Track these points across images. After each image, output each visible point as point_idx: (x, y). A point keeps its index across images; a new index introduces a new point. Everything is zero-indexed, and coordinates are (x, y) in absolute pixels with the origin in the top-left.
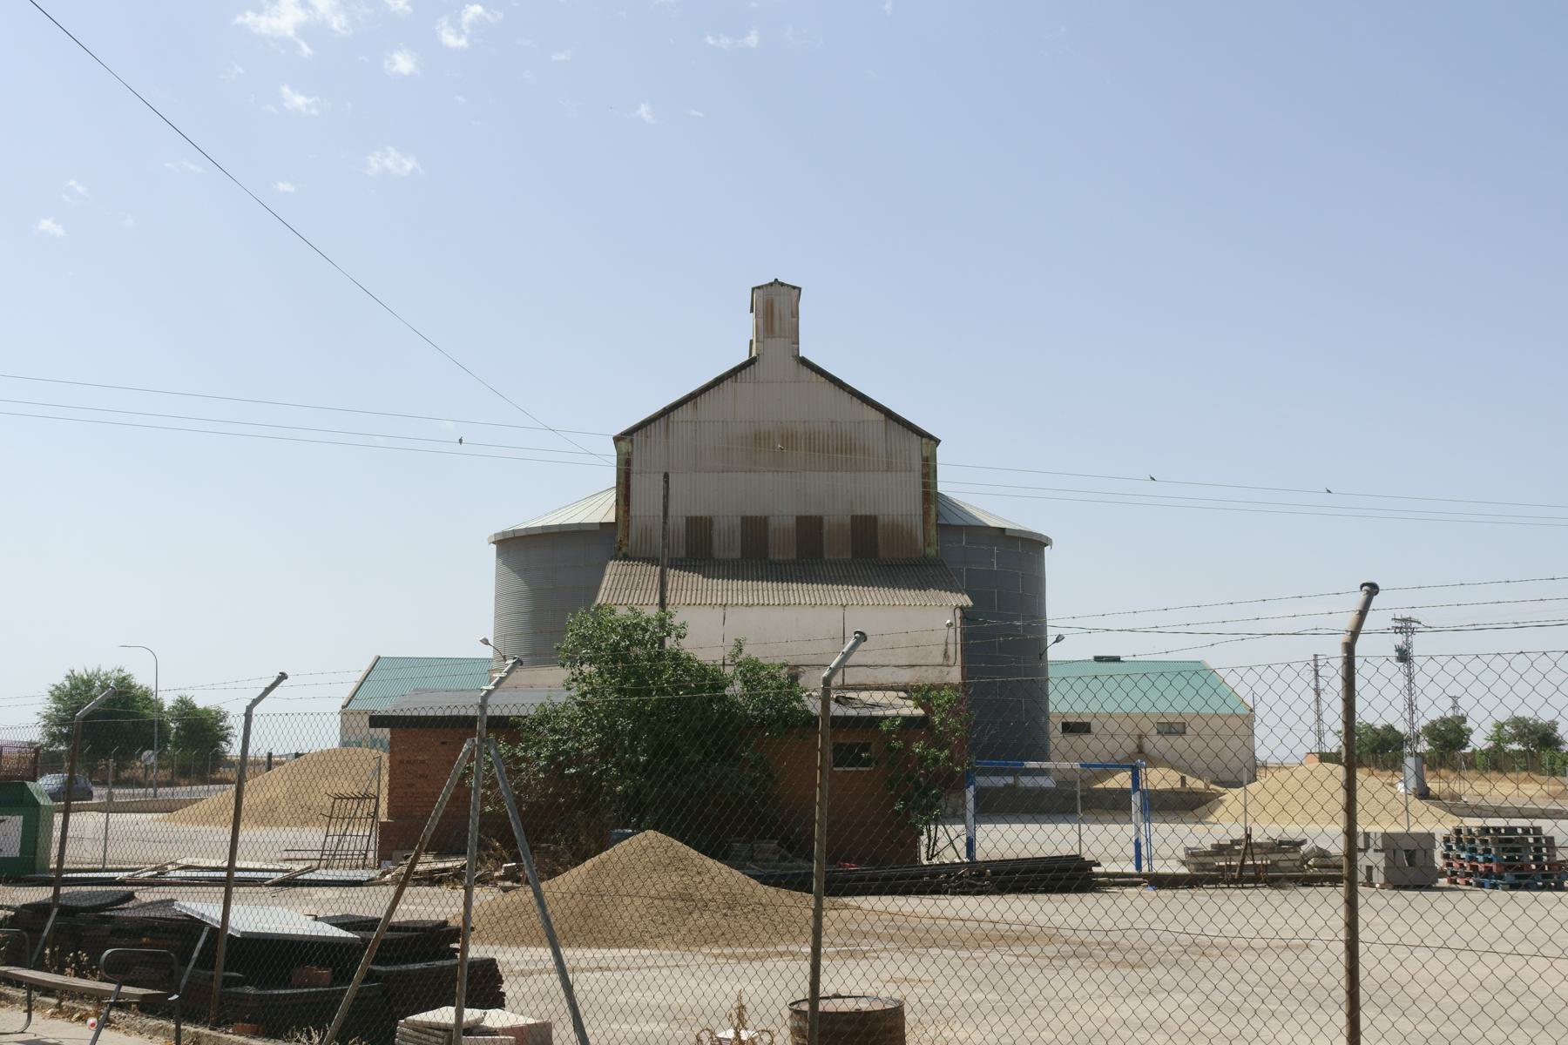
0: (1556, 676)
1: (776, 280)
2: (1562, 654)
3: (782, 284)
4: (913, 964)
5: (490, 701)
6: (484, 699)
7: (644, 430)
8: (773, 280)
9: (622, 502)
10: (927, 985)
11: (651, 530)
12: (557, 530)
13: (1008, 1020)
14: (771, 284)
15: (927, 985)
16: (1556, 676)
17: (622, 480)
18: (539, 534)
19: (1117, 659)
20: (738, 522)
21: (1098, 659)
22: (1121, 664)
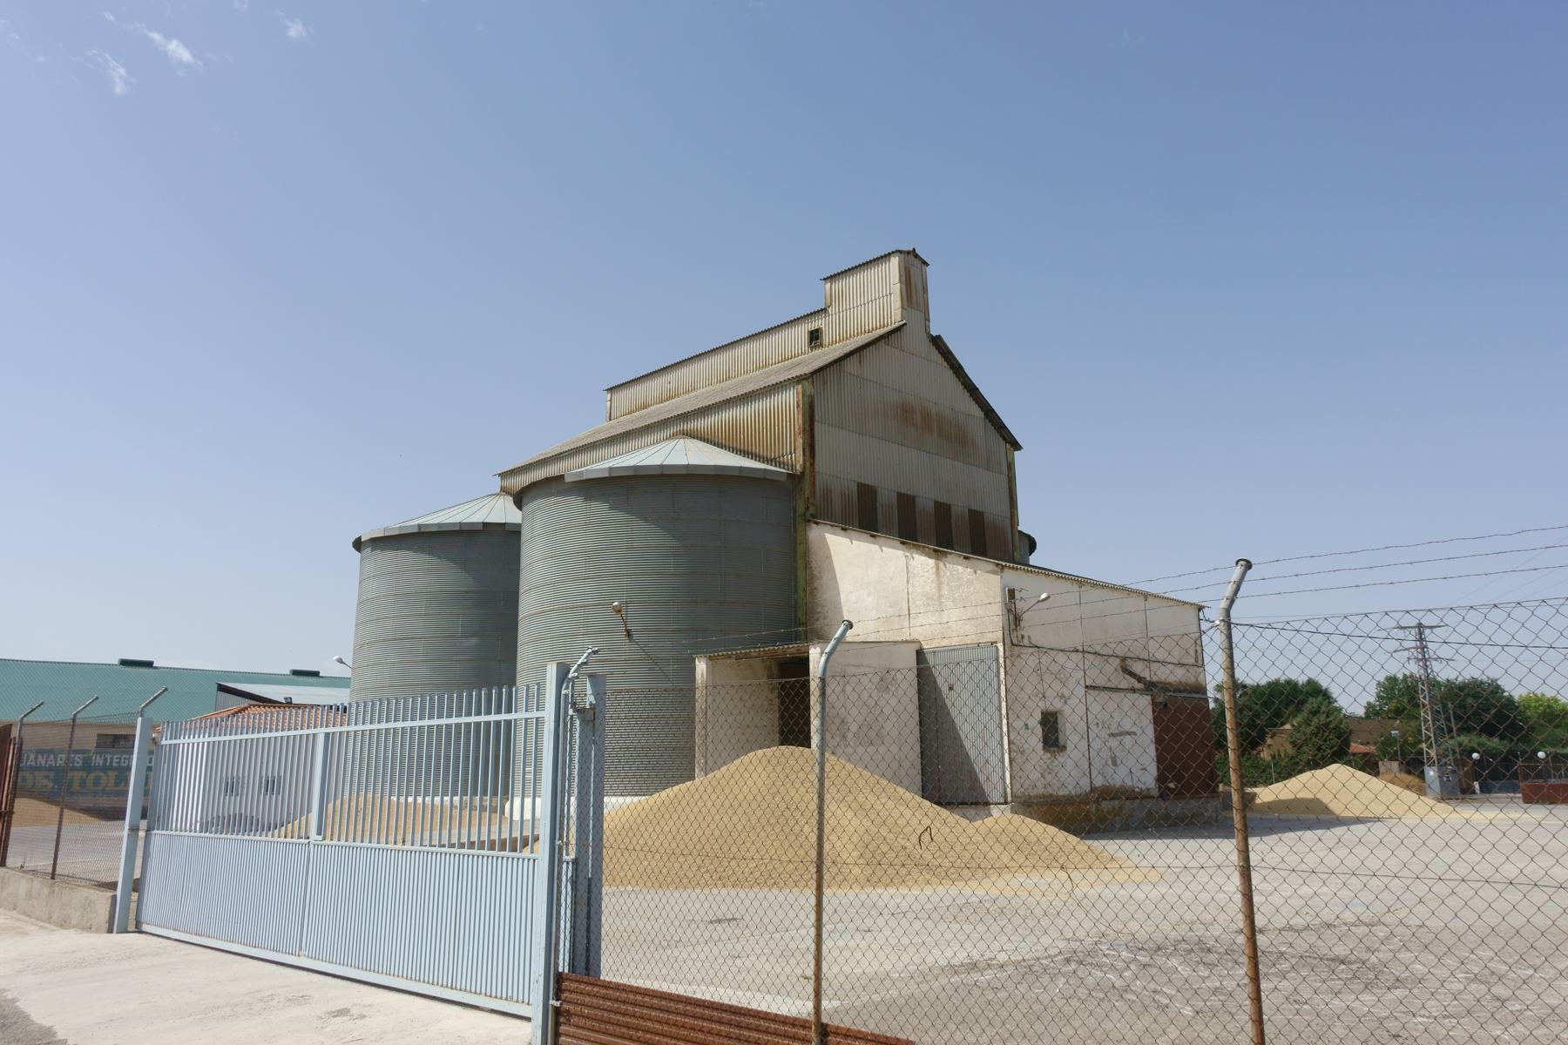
0: (1559, 622)
1: (914, 249)
2: (1321, 621)
3: (916, 256)
4: (1049, 880)
5: (78, 716)
6: (75, 715)
7: (821, 373)
8: (911, 249)
9: (808, 453)
10: (1211, 871)
11: (831, 492)
12: (736, 473)
13: (955, 926)
14: (908, 253)
15: (1194, 871)
16: (1559, 622)
17: (807, 427)
18: (760, 479)
19: (149, 664)
20: (854, 488)
21: (124, 663)
22: (151, 670)
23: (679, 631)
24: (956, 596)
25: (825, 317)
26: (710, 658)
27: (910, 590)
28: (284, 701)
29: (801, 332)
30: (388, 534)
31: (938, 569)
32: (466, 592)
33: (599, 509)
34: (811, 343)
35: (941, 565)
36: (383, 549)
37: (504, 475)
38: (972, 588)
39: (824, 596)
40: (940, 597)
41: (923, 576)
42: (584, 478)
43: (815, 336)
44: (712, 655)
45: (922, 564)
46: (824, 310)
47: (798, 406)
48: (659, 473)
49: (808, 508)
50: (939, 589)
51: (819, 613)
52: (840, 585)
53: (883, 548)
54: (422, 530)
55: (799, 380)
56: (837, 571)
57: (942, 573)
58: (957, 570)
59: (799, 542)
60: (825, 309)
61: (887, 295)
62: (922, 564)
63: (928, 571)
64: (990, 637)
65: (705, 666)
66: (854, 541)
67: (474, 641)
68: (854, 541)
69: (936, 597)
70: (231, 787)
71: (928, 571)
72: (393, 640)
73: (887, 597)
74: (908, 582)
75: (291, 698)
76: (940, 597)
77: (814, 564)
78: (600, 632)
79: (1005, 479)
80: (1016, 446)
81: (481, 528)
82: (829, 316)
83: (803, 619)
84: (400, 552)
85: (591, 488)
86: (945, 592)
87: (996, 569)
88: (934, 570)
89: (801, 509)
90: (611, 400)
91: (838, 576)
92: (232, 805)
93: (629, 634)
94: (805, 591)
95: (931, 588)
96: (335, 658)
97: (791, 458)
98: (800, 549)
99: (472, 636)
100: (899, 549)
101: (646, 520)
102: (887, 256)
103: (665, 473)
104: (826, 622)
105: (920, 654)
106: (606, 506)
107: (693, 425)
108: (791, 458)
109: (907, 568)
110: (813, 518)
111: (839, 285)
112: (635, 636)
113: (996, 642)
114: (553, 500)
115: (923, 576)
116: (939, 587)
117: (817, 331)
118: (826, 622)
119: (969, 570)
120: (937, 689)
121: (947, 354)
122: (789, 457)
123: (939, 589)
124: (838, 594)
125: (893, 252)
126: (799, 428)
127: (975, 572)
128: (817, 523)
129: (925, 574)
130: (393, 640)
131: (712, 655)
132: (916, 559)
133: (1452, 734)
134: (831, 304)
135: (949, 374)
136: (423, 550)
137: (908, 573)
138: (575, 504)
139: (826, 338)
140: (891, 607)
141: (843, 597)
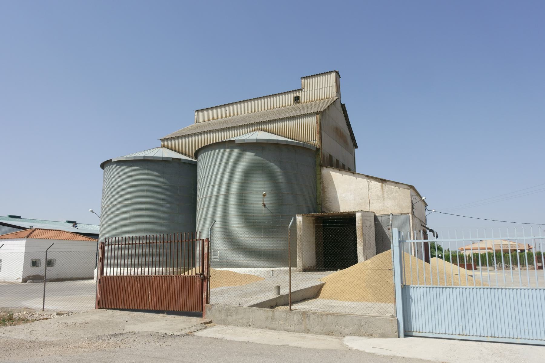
8: (337, 71)
23: (283, 205)
24: (391, 196)
25: (301, 92)
26: (303, 216)
27: (370, 194)
28: (29, 228)
29: (291, 97)
30: (127, 159)
31: (382, 186)
32: (164, 185)
33: (250, 155)
34: (295, 101)
35: (384, 185)
36: (123, 166)
37: (163, 140)
38: (398, 194)
39: (329, 194)
40: (383, 196)
41: (375, 189)
42: (245, 142)
43: (297, 99)
44: (304, 214)
45: (375, 185)
46: (301, 90)
47: (317, 123)
48: (276, 143)
49: (321, 161)
50: (383, 194)
51: (327, 201)
52: (337, 191)
53: (357, 178)
54: (145, 159)
55: (317, 113)
56: (336, 185)
57: (384, 188)
58: (391, 187)
59: (317, 174)
60: (302, 89)
61: (323, 88)
62: (375, 185)
63: (378, 187)
64: (406, 211)
65: (301, 218)
66: (343, 175)
67: (168, 205)
68: (343, 175)
69: (381, 197)
70: (35, 264)
71: (378, 187)
72: (130, 203)
73: (359, 196)
74: (369, 191)
75: (33, 227)
76: (383, 196)
77: (325, 182)
78: (252, 204)
79: (354, 157)
80: (356, 146)
81: (171, 160)
82: (303, 92)
83: (320, 203)
84: (133, 167)
85: (246, 146)
86: (386, 194)
87: (409, 187)
88: (381, 187)
89: (318, 162)
90: (197, 115)
91: (336, 187)
92: (39, 271)
93: (264, 205)
94: (320, 192)
95: (379, 193)
96: (90, 210)
97: (314, 142)
98: (318, 177)
99: (167, 203)
100: (365, 179)
101: (270, 161)
102: (330, 72)
103: (279, 143)
104: (331, 204)
105: (375, 217)
106: (254, 154)
107: (264, 127)
108: (314, 142)
109: (368, 186)
110: (322, 166)
111: (307, 81)
112: (267, 206)
113: (408, 214)
114: (226, 150)
115: (375, 189)
116: (383, 193)
117: (298, 97)
118: (331, 204)
119: (396, 187)
120: (382, 229)
121: (345, 111)
122: (313, 142)
123: (383, 194)
124: (336, 194)
125: (333, 71)
126: (318, 131)
127: (399, 188)
128: (326, 167)
129: (376, 188)
130: (130, 203)
131: (304, 214)
132: (372, 182)
133: (513, 254)
134: (304, 88)
135: (344, 118)
136: (145, 167)
137: (369, 187)
138: (238, 152)
139: (302, 100)
140: (361, 199)
141: (338, 195)
